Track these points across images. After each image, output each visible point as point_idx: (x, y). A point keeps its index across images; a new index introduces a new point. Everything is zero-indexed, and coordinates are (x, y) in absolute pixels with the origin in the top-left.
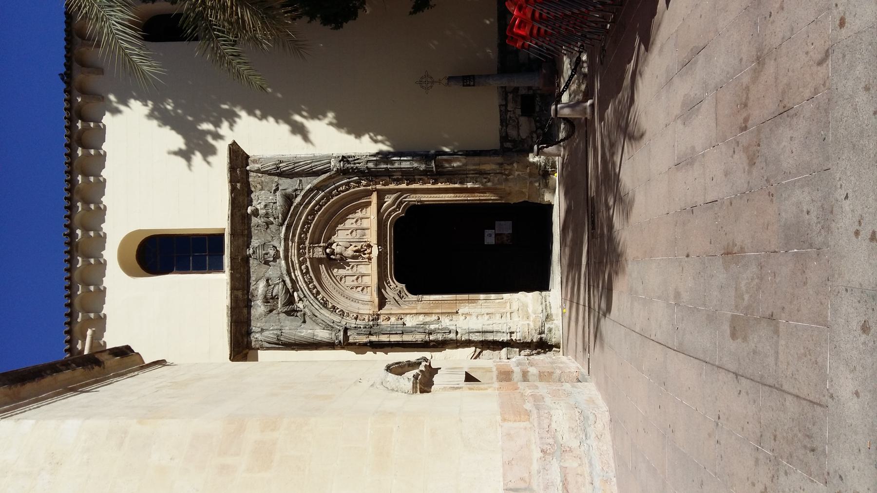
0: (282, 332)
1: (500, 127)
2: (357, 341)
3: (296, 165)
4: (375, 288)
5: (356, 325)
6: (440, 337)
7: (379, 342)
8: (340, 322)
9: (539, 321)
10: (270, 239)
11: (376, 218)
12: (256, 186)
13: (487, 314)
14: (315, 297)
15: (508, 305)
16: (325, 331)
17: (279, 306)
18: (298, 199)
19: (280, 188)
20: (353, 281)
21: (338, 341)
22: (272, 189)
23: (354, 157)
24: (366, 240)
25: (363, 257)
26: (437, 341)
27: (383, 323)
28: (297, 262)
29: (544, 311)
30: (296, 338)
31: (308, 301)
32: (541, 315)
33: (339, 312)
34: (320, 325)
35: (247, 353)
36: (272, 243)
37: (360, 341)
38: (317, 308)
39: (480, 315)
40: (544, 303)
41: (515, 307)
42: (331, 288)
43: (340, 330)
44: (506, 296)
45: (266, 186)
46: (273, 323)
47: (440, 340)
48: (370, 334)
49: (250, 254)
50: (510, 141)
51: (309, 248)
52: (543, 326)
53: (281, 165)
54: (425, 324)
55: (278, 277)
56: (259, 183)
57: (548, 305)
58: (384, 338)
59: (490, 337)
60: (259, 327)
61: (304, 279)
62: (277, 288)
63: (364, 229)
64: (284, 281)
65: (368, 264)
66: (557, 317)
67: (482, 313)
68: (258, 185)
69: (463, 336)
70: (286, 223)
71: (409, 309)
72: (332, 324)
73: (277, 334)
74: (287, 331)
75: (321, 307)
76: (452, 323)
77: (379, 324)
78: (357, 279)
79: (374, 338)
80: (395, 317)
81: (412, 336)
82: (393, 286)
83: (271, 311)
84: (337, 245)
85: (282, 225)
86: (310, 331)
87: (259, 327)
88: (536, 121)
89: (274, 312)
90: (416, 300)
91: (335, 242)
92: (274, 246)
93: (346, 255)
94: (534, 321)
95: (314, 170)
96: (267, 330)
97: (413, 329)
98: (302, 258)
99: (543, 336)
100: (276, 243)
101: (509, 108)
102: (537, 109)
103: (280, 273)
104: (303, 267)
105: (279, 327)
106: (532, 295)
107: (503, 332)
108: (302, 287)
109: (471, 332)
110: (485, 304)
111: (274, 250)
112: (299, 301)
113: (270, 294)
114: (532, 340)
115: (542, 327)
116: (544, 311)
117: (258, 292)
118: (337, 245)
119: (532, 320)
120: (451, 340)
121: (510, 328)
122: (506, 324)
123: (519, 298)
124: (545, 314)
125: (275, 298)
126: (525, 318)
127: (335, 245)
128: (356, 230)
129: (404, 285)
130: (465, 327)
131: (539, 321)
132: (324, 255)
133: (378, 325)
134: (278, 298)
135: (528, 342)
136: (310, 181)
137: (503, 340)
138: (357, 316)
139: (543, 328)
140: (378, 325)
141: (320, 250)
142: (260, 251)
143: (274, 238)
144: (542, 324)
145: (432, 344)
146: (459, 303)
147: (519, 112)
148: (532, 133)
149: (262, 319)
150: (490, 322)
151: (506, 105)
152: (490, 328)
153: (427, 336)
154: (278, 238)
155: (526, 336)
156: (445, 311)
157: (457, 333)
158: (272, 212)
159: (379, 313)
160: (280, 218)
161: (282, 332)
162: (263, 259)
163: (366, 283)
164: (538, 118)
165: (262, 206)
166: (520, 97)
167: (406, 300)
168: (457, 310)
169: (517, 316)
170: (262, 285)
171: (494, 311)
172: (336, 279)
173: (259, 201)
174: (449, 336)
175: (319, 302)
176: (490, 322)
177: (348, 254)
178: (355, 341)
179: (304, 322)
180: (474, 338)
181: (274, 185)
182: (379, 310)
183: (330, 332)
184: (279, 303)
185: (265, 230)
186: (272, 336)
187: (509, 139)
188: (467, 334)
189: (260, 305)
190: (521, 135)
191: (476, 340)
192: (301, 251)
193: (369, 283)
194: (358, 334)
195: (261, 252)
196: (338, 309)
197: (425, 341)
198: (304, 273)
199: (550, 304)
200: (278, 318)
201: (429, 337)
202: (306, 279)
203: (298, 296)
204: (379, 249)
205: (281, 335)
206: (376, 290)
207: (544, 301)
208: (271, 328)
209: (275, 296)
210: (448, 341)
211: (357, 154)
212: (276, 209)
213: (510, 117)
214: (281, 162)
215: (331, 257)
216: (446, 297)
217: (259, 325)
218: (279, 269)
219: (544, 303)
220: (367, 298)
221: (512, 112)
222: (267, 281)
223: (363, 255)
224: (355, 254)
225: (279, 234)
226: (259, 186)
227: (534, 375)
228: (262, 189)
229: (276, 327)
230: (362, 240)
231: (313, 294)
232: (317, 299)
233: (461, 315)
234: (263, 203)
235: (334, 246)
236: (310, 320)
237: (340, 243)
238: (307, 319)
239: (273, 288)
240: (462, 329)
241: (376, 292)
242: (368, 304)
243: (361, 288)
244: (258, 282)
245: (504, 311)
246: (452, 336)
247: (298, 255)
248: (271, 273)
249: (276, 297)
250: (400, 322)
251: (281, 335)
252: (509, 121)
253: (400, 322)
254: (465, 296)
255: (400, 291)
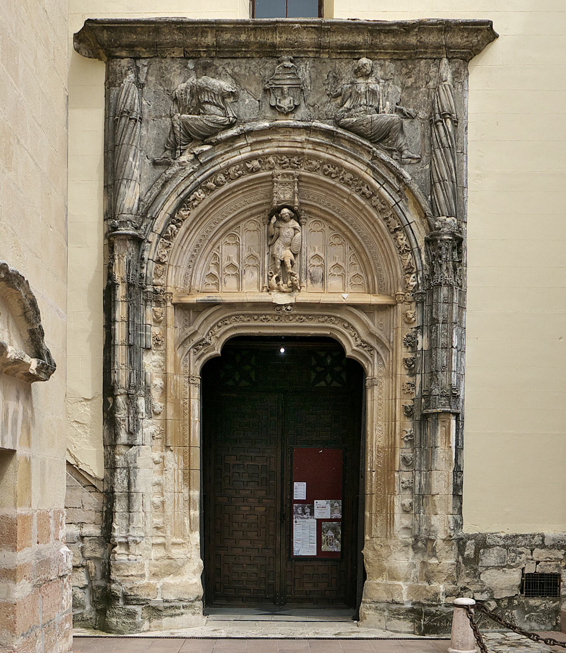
0: (136, 121)
1: (503, 535)
2: (117, 261)
3: (448, 150)
4: (215, 298)
5: (146, 260)
6: (121, 415)
7: (115, 301)
8: (152, 231)
9: (149, 595)
10: (311, 101)
11: (344, 301)
12: (410, 77)
13: (163, 503)
14: (200, 183)
15: (179, 540)
16: (137, 201)
17: (185, 116)
18: (384, 156)
19: (406, 122)
20: (229, 258)
21: (117, 224)
22: (403, 106)
23: (460, 262)
24: (304, 284)
25: (272, 277)
26: (114, 409)
27: (149, 310)
28: (267, 151)
29: (167, 605)
30: (124, 147)
31: (192, 170)
32: (159, 599)
33: (172, 229)
34: (149, 194)
35: (100, 59)
36: (303, 105)
37: (117, 266)
38: (180, 190)
39: (162, 490)
40: (181, 604)
41: (176, 552)
42: (216, 218)
43: (136, 228)
44: (196, 537)
45: (409, 95)
46: (154, 105)
47: (116, 415)
48: (130, 286)
49: (283, 61)
50: (477, 552)
51: (292, 174)
52: (138, 601)
53: (448, 121)
54: (148, 391)
55: (238, 116)
56: (415, 82)
57: (178, 611)
58: (121, 312)
59: (120, 507)
60: (146, 79)
61: (234, 164)
62: (219, 111)
63: (323, 279)
64: (231, 126)
65: (258, 287)
66: (155, 627)
67: (165, 494)
68: (412, 80)
69: (122, 458)
70: (340, 131)
71: (175, 361)
72: (149, 216)
73: (133, 110)
74: (138, 130)
75: (182, 196)
76: (149, 439)
77: (149, 303)
78: (232, 266)
79: (121, 292)
80: (160, 334)
81: (124, 363)
82: (218, 332)
83: (175, 100)
84: (295, 229)
85: (337, 123)
86: (137, 173)
87: (146, 79)
88: (511, 599)
89: (174, 108)
90: (191, 374)
91: (300, 225)
92: (296, 107)
93: (277, 245)
94: (148, 586)
95: (438, 185)
96: (141, 94)
97: (136, 365)
98: (273, 161)
99: (121, 603)
100: (302, 112)
101: (537, 550)
102: (533, 602)
103: (246, 119)
104: (256, 163)
105: (145, 116)
106: (196, 583)
107: (128, 531)
108: (220, 160)
109: (129, 471)
110: (181, 499)
111: (289, 108)
112: (194, 153)
113: (206, 99)
114: (114, 582)
115: (138, 600)
116: (167, 605)
117: (213, 78)
118: (295, 229)
119: (152, 582)
120: (116, 435)
121: (136, 542)
122: (143, 535)
123: (191, 561)
124: (161, 605)
125: (199, 108)
126: (154, 570)
127: (297, 225)
128: (323, 266)
129: (219, 353)
130: (140, 462)
131: (149, 595)
132: (278, 202)
133: (146, 301)
134: (199, 114)
135: (110, 574)
136: (417, 178)
137: (114, 528)
138: (163, 263)
139: (134, 602)
140: (146, 301)
141: (288, 196)
142: (288, 82)
143: (311, 108)
144: (144, 600)
145: (110, 399)
146: (184, 452)
147: (531, 569)
148: (491, 591)
149: (161, 85)
150: (148, 508)
151: (543, 546)
152: (137, 506)
153: (122, 391)
154: (313, 115)
155: (121, 572)
156: (169, 425)
157: (130, 446)
158: (361, 106)
159: (169, 304)
160: (348, 119)
161: (136, 121)
162: (273, 86)
163: (225, 283)
164: (516, 602)
165: (372, 86)
166: (556, 571)
167: (192, 354)
168: (171, 448)
169: (159, 555)
170: (226, 85)
171: (169, 514)
172: (232, 227)
173: (381, 81)
174: (123, 430)
175: (191, 192)
176: (148, 508)
177: (278, 249)
178: (116, 257)
179: (155, 164)
180: (119, 477)
181: (411, 110)
182: (175, 305)
183: (134, 211)
184: (190, 116)
185: (328, 92)
186: (129, 101)
187: (482, 551)
188: (125, 465)
189: (189, 81)
190: (488, 572)
191: (116, 480)
192: (287, 160)
193: (222, 288)
194: (129, 263)
195: (286, 82)
196: (178, 227)
197: (114, 387)
198: (245, 165)
199: (179, 615)
200: (164, 114)
201: (121, 394)
202: (234, 168)
203: (202, 153)
204: (286, 305)
205: (130, 119)
206: (211, 298)
207: (185, 604)
208: (144, 102)
209: (203, 109)
210: (115, 429)
211: (465, 268)
212: (366, 112)
213: (521, 553)
214: (455, 123)
215: (274, 217)
216: (196, 428)
217: (151, 79)
218: (253, 117)
219: (181, 604)
220: (197, 283)
221: (530, 557)
222: (232, 94)
223: (275, 276)
224: (279, 261)
225: (319, 119)
226: (410, 82)
227: (8, 593)
228: (404, 87)
229: (146, 110)
230: (303, 275)
231: (205, 180)
232: (195, 189)
233: (162, 454)
234: (379, 88)
235: (293, 223)
236: (157, 175)
237: (299, 234)
238: (160, 170)
239: (217, 106)
240: (135, 455)
241: (206, 298)
242: (185, 284)
243: (215, 272)
244: (230, 79)
245: (168, 533)
246: (123, 437)
247: (277, 153)
248: (247, 101)
249: (202, 111)
250: (151, 343)
251: (130, 119)
252: (514, 551)
253: (151, 343)
254: (196, 463)
255: (207, 344)
